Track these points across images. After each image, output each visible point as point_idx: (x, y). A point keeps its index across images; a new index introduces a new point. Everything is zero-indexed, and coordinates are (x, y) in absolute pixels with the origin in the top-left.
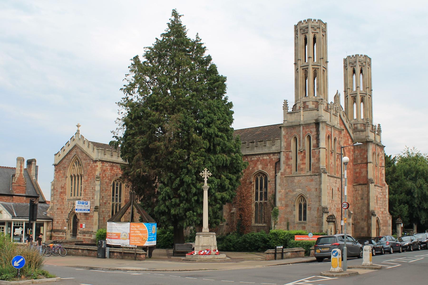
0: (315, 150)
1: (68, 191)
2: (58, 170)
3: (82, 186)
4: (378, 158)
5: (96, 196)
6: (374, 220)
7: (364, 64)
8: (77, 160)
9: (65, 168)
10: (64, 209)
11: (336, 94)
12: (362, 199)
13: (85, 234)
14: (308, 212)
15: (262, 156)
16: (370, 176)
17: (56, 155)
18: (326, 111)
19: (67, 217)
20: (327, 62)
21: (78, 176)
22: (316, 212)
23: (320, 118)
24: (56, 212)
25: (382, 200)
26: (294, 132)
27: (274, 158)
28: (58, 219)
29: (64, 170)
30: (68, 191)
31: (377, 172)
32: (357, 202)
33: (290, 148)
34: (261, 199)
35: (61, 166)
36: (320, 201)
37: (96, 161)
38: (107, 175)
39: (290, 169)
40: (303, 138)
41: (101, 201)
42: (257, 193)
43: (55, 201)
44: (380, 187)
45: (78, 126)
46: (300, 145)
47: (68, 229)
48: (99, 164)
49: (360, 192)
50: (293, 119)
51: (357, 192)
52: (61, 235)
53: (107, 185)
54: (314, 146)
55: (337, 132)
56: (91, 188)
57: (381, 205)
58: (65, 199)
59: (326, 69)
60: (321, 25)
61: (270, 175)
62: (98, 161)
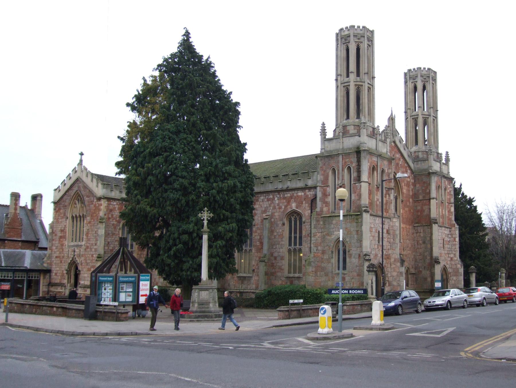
0: (357, 184)
1: (68, 234)
2: (57, 209)
3: (84, 229)
4: (445, 193)
5: (98, 242)
6: (438, 270)
7: (427, 79)
8: (79, 198)
9: (66, 206)
10: (63, 257)
11: (391, 116)
12: (424, 242)
13: (86, 289)
14: (348, 260)
15: (296, 192)
16: (434, 214)
17: (55, 190)
18: (370, 137)
19: (67, 267)
20: (373, 78)
21: (80, 216)
22: (357, 260)
23: (362, 145)
24: (54, 262)
25: (451, 243)
26: (333, 163)
27: (310, 194)
28: (57, 270)
29: (64, 209)
30: (68, 234)
31: (444, 210)
32: (419, 247)
33: (327, 182)
34: (295, 244)
35: (61, 204)
36: (361, 246)
37: (99, 199)
38: (114, 216)
39: (327, 208)
40: (343, 170)
41: (106, 248)
42: (290, 238)
43: (54, 248)
44: (447, 228)
45: (82, 154)
46: (338, 178)
47: (68, 283)
48: (104, 203)
49: (422, 235)
50: (332, 146)
51: (418, 234)
52: (59, 289)
53: (115, 228)
54: (354, 180)
55: (386, 163)
56: (94, 232)
57: (449, 249)
58: (64, 245)
59: (373, 86)
60: (365, 33)
61: (305, 215)
62: (102, 198)
